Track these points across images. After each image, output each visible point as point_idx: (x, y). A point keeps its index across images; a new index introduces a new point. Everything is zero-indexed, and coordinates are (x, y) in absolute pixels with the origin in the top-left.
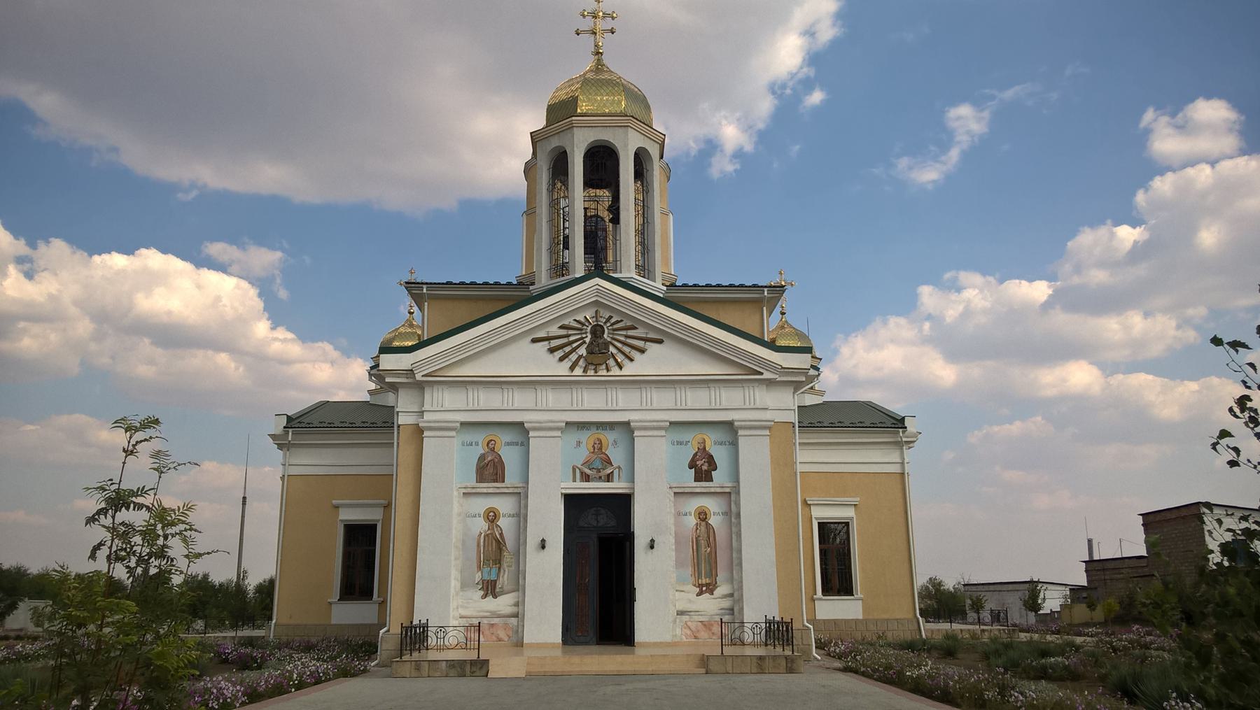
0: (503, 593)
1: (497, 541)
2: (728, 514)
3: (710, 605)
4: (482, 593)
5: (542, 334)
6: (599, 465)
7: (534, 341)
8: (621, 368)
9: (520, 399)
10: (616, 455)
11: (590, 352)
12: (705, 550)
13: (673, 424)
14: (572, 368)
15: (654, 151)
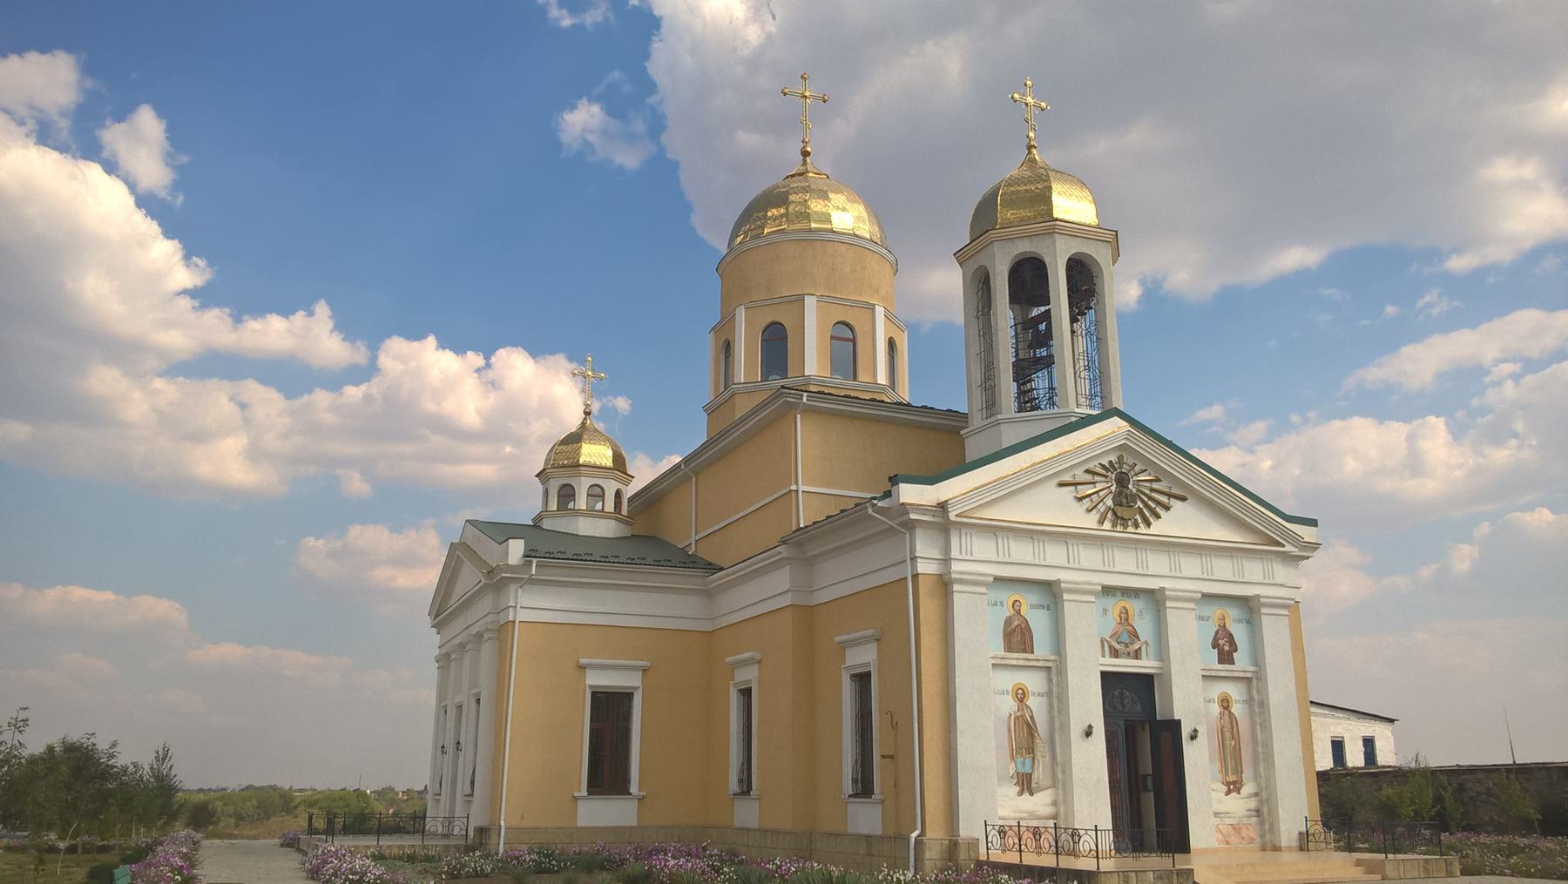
0: (1040, 789)
1: (1028, 725)
2: (1249, 701)
3: (1039, 804)
4: (1017, 789)
5: (1067, 478)
6: (1123, 641)
7: (1061, 485)
8: (1148, 524)
9: (1055, 553)
10: (1144, 627)
11: (1118, 503)
12: (1230, 743)
13: (999, 580)
14: (1101, 522)
15: (1100, 254)
